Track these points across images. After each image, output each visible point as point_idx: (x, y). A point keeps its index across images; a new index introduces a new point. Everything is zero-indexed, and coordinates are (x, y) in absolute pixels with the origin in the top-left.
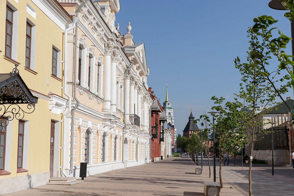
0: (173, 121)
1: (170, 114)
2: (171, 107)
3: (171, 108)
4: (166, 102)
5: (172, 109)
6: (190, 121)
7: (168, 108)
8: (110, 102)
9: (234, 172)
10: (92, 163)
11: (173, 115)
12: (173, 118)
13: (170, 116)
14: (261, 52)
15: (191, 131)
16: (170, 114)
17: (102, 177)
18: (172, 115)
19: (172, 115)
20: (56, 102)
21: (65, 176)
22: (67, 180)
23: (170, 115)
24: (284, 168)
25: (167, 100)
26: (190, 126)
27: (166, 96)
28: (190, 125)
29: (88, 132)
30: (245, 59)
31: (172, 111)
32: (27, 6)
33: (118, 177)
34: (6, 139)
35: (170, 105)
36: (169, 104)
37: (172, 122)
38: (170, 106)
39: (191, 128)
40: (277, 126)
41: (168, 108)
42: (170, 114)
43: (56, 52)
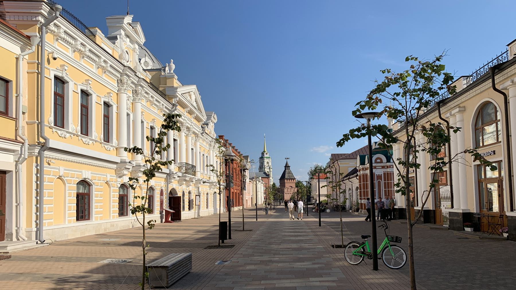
0: (271, 170)
1: (268, 163)
2: (269, 156)
3: (269, 158)
5: (270, 159)
6: (285, 169)
7: (267, 158)
8: (243, 229)
10: (201, 210)
11: (271, 165)
12: (271, 167)
13: (268, 166)
15: (287, 179)
16: (268, 163)
17: (96, 244)
18: (271, 165)
19: (270, 164)
20: (54, 75)
21: (24, 240)
22: (77, 243)
23: (268, 165)
25: (266, 151)
26: (286, 174)
27: (264, 146)
28: (286, 173)
29: (207, 194)
31: (270, 161)
32: (102, 43)
33: (178, 235)
36: (267, 154)
37: (270, 171)
38: (268, 156)
41: (267, 158)
42: (268, 163)
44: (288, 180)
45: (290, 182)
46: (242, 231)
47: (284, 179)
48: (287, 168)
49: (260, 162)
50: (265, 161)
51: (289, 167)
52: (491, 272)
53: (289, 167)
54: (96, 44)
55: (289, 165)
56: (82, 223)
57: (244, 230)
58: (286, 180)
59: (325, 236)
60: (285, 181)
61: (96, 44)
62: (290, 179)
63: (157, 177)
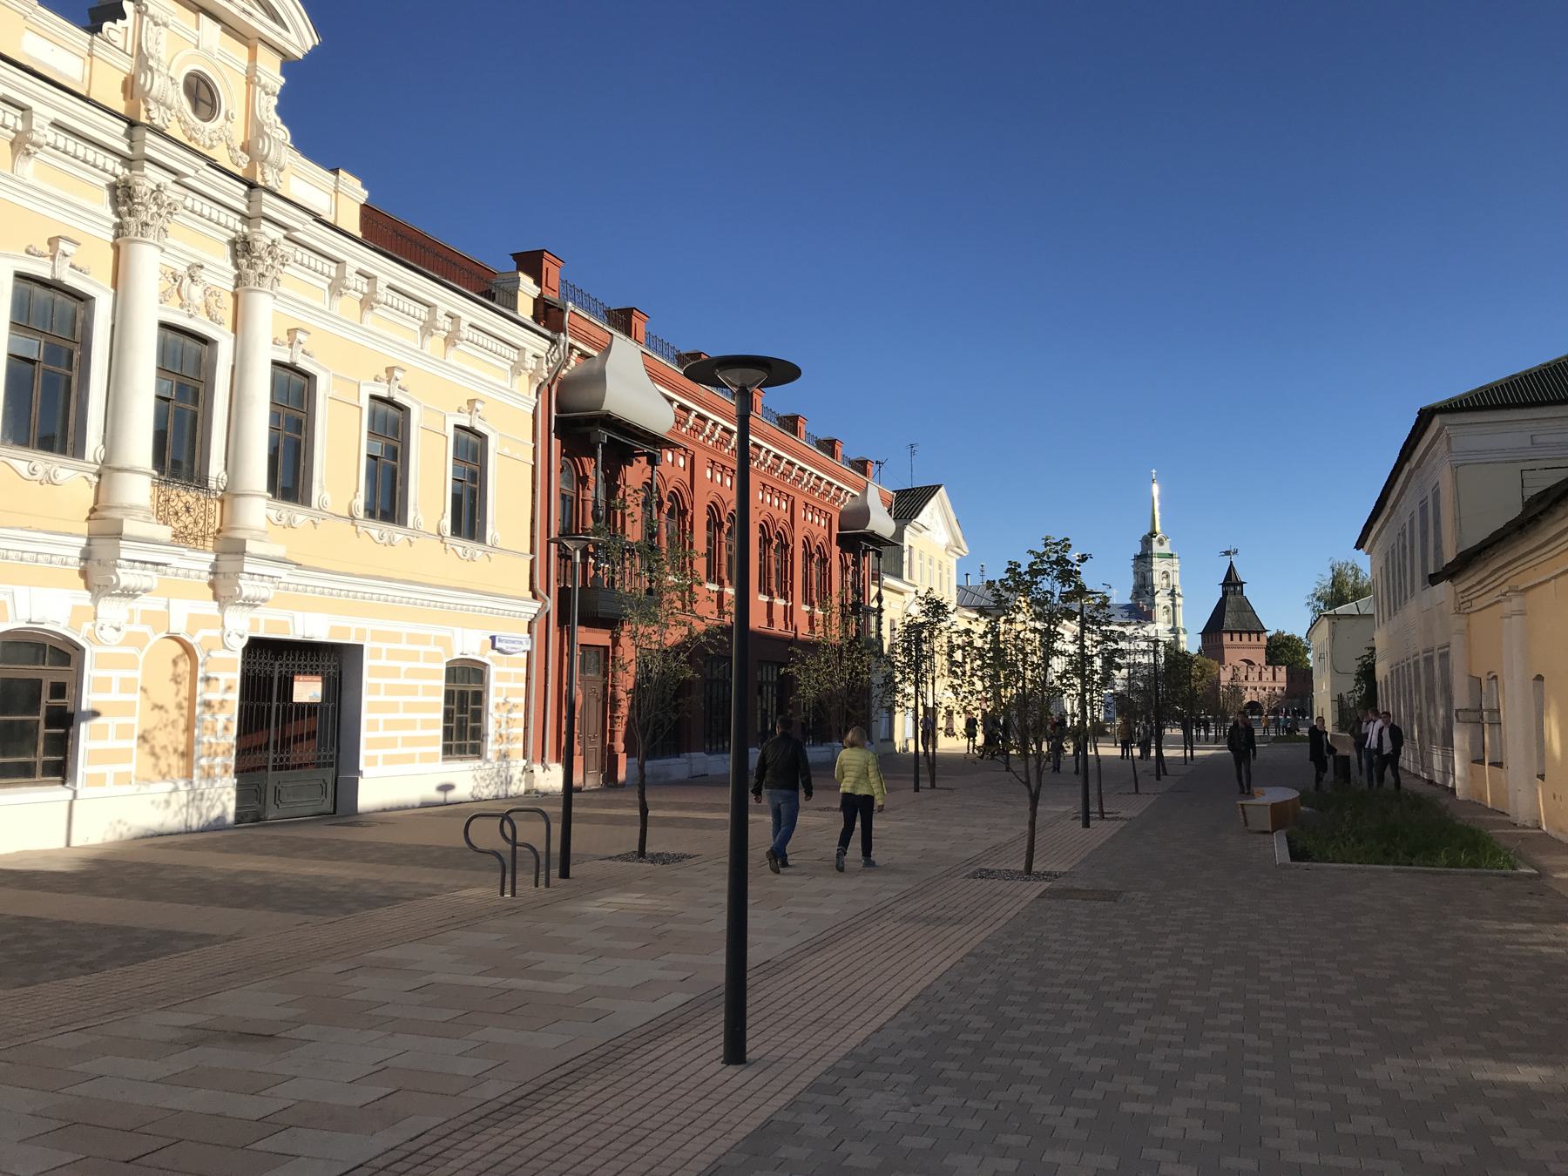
1: (1168, 577)
3: (1171, 556)
4: (1153, 534)
5: (1176, 561)
6: (1225, 593)
7: (1161, 556)
9: (230, 647)
14: (271, 671)
24: (1437, 693)
28: (1227, 609)
30: (547, 770)
34: (233, 320)
35: (1167, 544)
36: (1161, 542)
38: (1166, 549)
39: (1229, 621)
40: (1389, 754)
41: (1161, 556)
42: (1166, 575)
43: (89, 37)
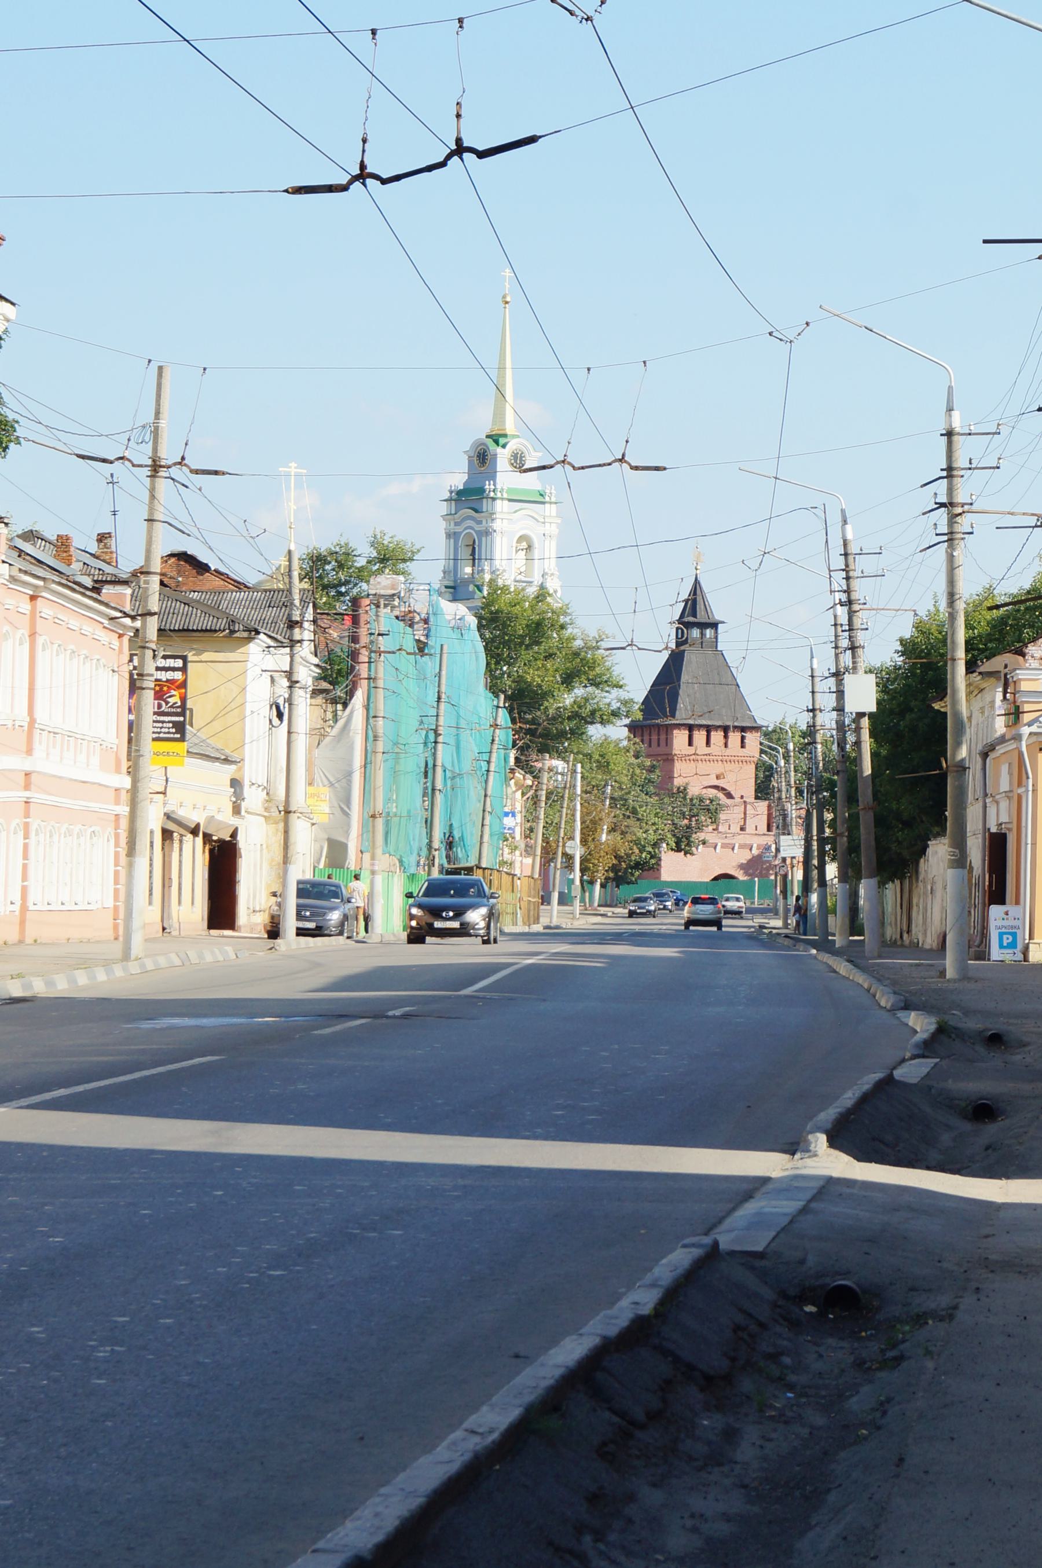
1: (529, 548)
44: (700, 736)
45: (728, 752)
46: (829, 569)
47: (669, 729)
48: (695, 633)
49: (449, 536)
50: (497, 525)
51: (714, 625)
52: (925, 978)
53: (714, 625)
54: (440, 670)
55: (718, 616)
56: (294, 931)
57: (830, 571)
58: (680, 738)
59: (840, 1275)
60: (669, 742)
61: (440, 670)
62: (717, 728)
63: (194, 841)
